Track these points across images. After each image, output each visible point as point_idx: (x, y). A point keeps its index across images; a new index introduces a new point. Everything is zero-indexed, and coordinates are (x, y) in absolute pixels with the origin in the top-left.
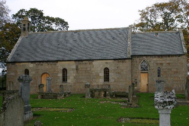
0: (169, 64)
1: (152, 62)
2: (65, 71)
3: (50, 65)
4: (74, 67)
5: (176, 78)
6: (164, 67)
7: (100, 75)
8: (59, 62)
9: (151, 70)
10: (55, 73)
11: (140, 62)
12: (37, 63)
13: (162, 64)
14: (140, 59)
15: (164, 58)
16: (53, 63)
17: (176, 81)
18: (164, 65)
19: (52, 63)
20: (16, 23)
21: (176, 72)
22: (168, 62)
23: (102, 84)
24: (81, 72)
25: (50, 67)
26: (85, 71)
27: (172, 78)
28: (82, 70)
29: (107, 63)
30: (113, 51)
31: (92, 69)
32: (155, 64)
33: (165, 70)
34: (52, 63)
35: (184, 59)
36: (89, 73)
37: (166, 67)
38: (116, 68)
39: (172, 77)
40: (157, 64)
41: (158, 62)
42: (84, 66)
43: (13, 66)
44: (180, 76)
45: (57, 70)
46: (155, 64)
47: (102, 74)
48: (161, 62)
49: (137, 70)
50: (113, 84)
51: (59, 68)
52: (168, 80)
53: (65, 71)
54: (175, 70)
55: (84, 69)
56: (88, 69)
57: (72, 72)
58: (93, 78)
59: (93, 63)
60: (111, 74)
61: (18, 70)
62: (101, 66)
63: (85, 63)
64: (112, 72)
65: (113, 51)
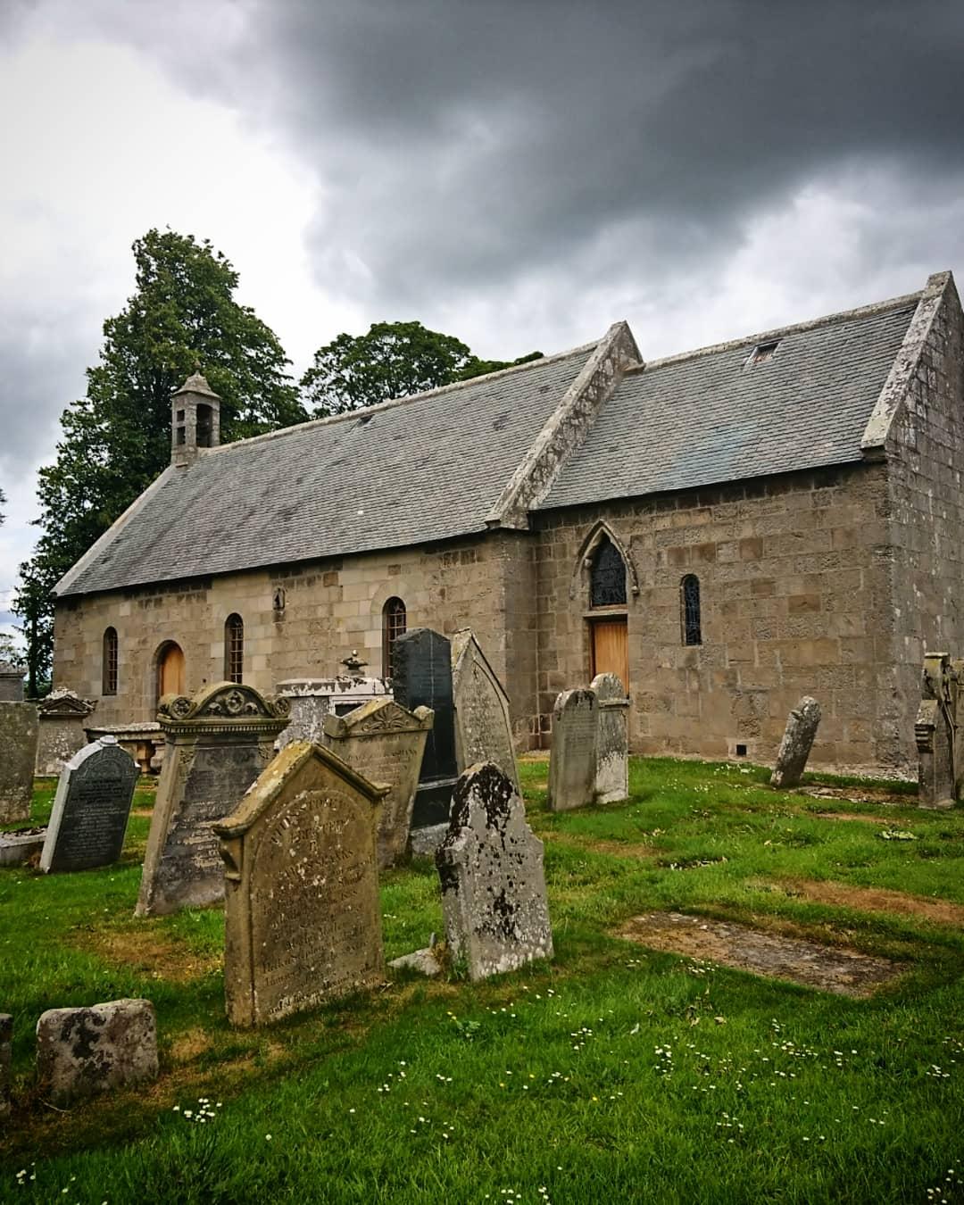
1: (649, 543)
13: (707, 552)
18: (724, 554)
38: (438, 599)
40: (679, 555)
46: (665, 557)
54: (798, 590)
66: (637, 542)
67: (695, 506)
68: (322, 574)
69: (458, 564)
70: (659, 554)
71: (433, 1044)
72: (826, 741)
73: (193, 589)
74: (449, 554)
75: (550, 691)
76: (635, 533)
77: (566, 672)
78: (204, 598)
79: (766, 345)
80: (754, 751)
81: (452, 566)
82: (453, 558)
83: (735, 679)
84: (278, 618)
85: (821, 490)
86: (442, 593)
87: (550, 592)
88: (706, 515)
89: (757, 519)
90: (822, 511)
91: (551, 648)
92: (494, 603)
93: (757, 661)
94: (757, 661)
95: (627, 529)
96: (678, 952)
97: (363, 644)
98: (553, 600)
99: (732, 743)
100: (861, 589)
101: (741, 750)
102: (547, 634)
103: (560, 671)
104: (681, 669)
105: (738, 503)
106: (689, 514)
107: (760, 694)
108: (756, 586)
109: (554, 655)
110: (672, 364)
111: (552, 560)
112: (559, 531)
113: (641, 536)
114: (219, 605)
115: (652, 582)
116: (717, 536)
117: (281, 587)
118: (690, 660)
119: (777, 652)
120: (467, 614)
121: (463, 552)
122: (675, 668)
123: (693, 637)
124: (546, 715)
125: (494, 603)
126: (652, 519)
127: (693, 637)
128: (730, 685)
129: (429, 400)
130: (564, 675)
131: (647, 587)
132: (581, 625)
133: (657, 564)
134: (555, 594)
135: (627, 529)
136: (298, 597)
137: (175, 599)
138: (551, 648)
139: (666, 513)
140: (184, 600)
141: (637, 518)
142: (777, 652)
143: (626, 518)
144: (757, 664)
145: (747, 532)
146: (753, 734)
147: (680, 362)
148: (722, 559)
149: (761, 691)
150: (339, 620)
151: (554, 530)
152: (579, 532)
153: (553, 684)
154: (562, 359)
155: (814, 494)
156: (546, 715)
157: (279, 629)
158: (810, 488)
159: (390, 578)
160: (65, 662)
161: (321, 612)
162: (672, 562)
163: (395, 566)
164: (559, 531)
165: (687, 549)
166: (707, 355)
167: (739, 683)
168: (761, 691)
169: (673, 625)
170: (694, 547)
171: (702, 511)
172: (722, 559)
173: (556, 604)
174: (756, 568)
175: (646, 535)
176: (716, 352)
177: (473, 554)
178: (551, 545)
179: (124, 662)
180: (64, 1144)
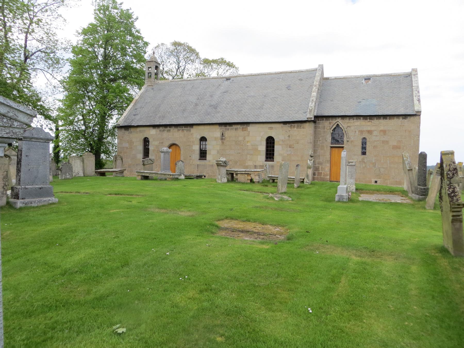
1: (352, 128)
2: (146, 141)
7: (259, 149)
11: (331, 129)
13: (370, 132)
18: (375, 133)
31: (247, 139)
32: (357, 132)
38: (287, 138)
40: (361, 132)
41: (365, 129)
46: (357, 132)
47: (263, 148)
48: (369, 129)
53: (146, 141)
54: (395, 144)
59: (248, 128)
60: (277, 148)
64: (280, 145)
66: (349, 128)
67: (367, 120)
68: (241, 127)
69: (295, 129)
70: (355, 131)
71: (186, 252)
72: (399, 180)
73: (184, 127)
74: (292, 126)
75: (317, 165)
76: (348, 125)
77: (323, 161)
78: (190, 131)
79: (368, 79)
80: (379, 182)
81: (293, 129)
82: (293, 127)
83: (376, 164)
84: (222, 139)
85: (403, 120)
86: (289, 136)
87: (319, 138)
88: (370, 123)
89: (385, 125)
90: (403, 125)
91: (318, 154)
92: (308, 141)
93: (382, 160)
94: (382, 160)
95: (346, 124)
96: (258, 225)
97: (257, 149)
98: (320, 141)
99: (373, 180)
100: (412, 145)
101: (376, 182)
102: (317, 150)
103: (321, 160)
104: (360, 162)
105: (380, 121)
106: (365, 122)
107: (382, 169)
108: (383, 142)
109: (319, 156)
110: (338, 79)
111: (320, 130)
112: (323, 122)
113: (350, 126)
114: (197, 133)
115: (353, 139)
116: (373, 128)
117: (224, 130)
118: (363, 159)
119: (388, 159)
120: (298, 143)
121: (297, 125)
122: (358, 161)
123: (364, 153)
124: (315, 172)
125: (308, 141)
126: (354, 122)
127: (364, 153)
128: (374, 166)
129: (253, 77)
130: (322, 161)
131: (351, 140)
132: (329, 148)
133: (355, 134)
134: (321, 139)
135: (346, 124)
136: (230, 133)
137: (177, 130)
138: (318, 154)
139: (358, 121)
140: (180, 131)
141: (349, 121)
142: (388, 159)
143: (346, 121)
144: (382, 161)
145: (382, 128)
146: (379, 178)
147: (341, 78)
148: (374, 134)
149: (383, 168)
150: (248, 141)
151: (321, 122)
152: (330, 123)
153: (318, 164)
154: (302, 71)
155: (401, 121)
156: (315, 172)
157: (223, 143)
158: (400, 119)
159: (269, 130)
160: (124, 147)
161: (241, 139)
162: (359, 134)
163: (271, 127)
164: (323, 122)
165: (364, 131)
166: (349, 78)
167: (377, 165)
168: (383, 168)
169: (359, 150)
170: (366, 130)
171: (369, 121)
172: (374, 134)
173: (321, 142)
174: (384, 137)
175: (352, 126)
176: (351, 78)
177: (301, 126)
178: (320, 126)
179: (153, 149)
180: (383, 287)
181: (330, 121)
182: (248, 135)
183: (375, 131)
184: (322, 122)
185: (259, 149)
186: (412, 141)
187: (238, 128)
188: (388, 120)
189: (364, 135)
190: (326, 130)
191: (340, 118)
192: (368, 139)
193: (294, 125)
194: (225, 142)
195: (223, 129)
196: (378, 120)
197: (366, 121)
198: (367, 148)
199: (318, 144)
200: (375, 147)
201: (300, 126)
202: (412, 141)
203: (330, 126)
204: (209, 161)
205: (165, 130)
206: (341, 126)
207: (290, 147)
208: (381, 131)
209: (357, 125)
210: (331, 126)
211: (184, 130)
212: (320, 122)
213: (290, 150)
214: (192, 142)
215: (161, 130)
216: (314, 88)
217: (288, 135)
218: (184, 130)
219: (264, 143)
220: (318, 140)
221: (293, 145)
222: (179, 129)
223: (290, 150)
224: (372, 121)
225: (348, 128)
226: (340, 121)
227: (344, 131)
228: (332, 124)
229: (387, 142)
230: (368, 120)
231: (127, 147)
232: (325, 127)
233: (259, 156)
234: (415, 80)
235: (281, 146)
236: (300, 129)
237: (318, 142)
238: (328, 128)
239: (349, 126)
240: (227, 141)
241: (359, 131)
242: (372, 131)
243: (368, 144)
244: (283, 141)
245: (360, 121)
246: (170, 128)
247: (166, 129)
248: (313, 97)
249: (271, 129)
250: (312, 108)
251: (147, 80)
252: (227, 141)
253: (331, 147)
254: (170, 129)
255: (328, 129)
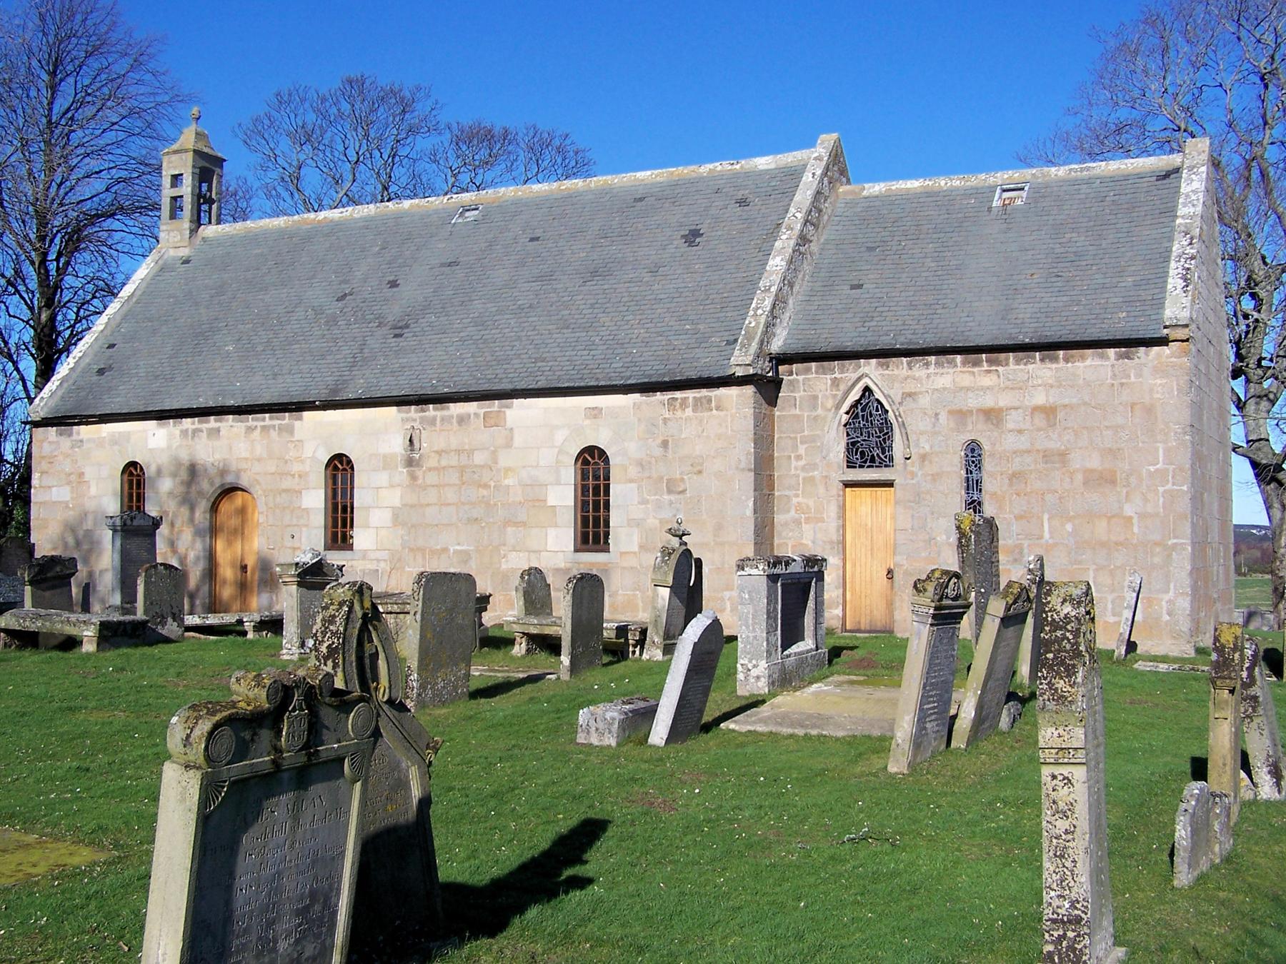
0: (1049, 412)
1: (924, 401)
2: (340, 467)
3: (257, 433)
4: (397, 445)
5: (1104, 523)
6: (1011, 442)
7: (551, 501)
8: (307, 415)
9: (913, 466)
10: (287, 483)
11: (838, 407)
12: (187, 423)
13: (992, 416)
14: (836, 383)
15: (1013, 366)
16: (276, 422)
17: (1103, 544)
18: (1012, 421)
19: (268, 422)
20: (581, 738)
21: (1103, 479)
22: (1040, 399)
23: (562, 565)
24: (432, 478)
25: (259, 450)
26: (462, 470)
27: (1069, 527)
28: (444, 463)
29: (595, 413)
30: (733, 304)
31: (505, 460)
32: (943, 417)
33: (1016, 465)
34: (268, 422)
35: (1159, 370)
36: (486, 486)
37: (1023, 443)
38: (658, 452)
39: (1070, 519)
40: (961, 415)
41: (973, 402)
42: (454, 443)
43: (65, 443)
44: (1129, 510)
45: (296, 468)
46: (943, 417)
47: (563, 496)
48: (988, 402)
49: (813, 466)
50: (633, 562)
51: (308, 451)
52: (1041, 537)
53: (340, 467)
54: (1094, 462)
55: (453, 460)
56: (479, 458)
57: (382, 478)
58: (508, 523)
59: (508, 412)
60: (621, 494)
61: (89, 473)
62: (560, 436)
63: (462, 420)
64: (631, 481)
65: (733, 304)
84: (410, 462)
86: (665, 444)
88: (994, 376)
105: (1030, 367)
106: (973, 373)
108: (1047, 456)
111: (797, 412)
113: (915, 394)
116: (1004, 401)
117: (416, 425)
126: (928, 376)
133: (934, 426)
139: (945, 370)
148: (1010, 425)
150: (508, 470)
157: (413, 477)
159: (587, 422)
165: (971, 412)
170: (979, 410)
171: (989, 372)
172: (1010, 425)
175: (921, 393)
181: (836, 375)
182: (509, 444)
183: (1013, 412)
184: (804, 380)
185: (551, 501)
186: (1161, 451)
187: (469, 416)
188: (1062, 364)
189: (970, 427)
190: (820, 411)
191: (874, 361)
192: (986, 446)
193: (684, 395)
194: (419, 473)
195: (415, 420)
196: (1022, 367)
197: (976, 370)
198: (987, 485)
199: (793, 472)
200: (1015, 477)
201: (704, 401)
202: (1161, 451)
203: (835, 396)
204: (364, 555)
205: (202, 431)
206: (878, 395)
207: (670, 492)
208: (1036, 409)
209: (940, 386)
210: (840, 394)
211: (272, 431)
212: (798, 381)
213: (671, 503)
214: (300, 476)
215: (187, 430)
216: (784, 237)
217: (659, 441)
218: (272, 431)
219: (569, 475)
220: (790, 457)
221: (682, 480)
222: (251, 423)
223: (671, 503)
224: (1000, 369)
225: (909, 403)
226: (870, 370)
227: (891, 414)
228: (843, 387)
229: (1063, 456)
230: (985, 366)
231: (67, 503)
232: (816, 397)
233: (552, 532)
234: (1189, 189)
235: (634, 485)
236: (706, 414)
237: (794, 463)
238: (830, 404)
239: (910, 395)
240: (430, 469)
241: (951, 412)
242: (1001, 410)
243: (988, 465)
244: (640, 464)
245: (951, 371)
246: (220, 421)
247: (204, 426)
248: (772, 273)
249: (595, 417)
250: (758, 324)
251: (169, 227)
252: (430, 469)
253: (848, 485)
254: (218, 424)
255: (830, 410)
